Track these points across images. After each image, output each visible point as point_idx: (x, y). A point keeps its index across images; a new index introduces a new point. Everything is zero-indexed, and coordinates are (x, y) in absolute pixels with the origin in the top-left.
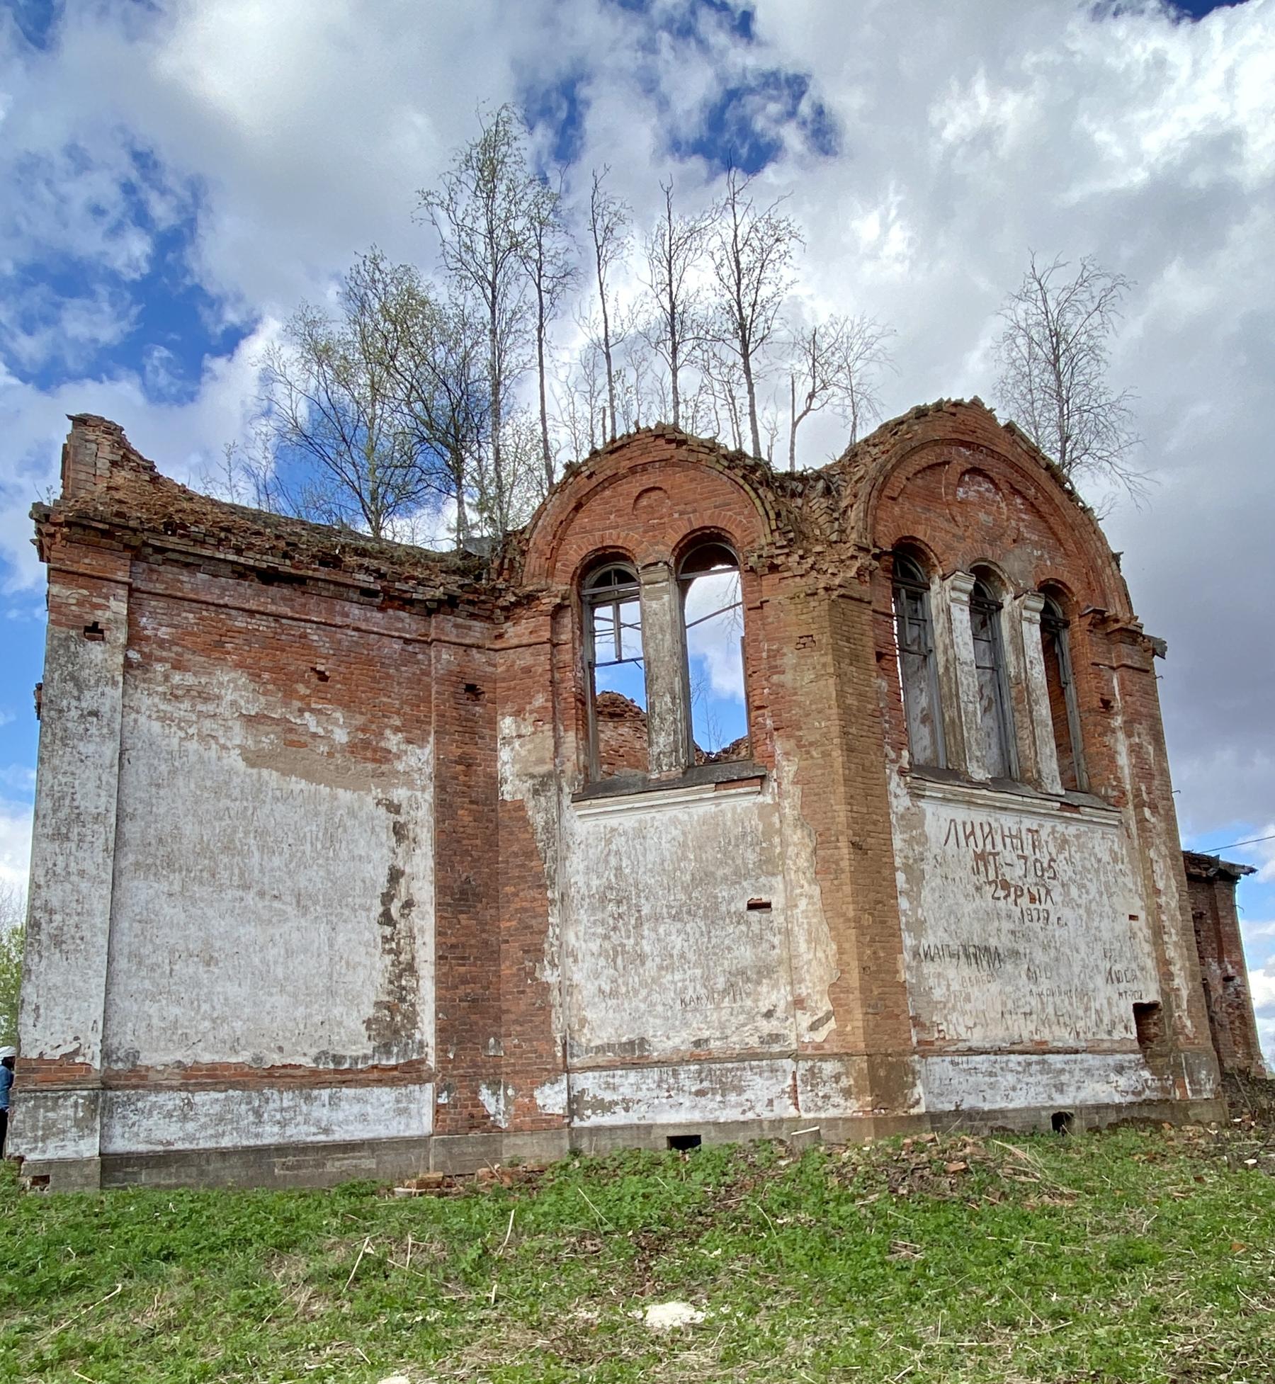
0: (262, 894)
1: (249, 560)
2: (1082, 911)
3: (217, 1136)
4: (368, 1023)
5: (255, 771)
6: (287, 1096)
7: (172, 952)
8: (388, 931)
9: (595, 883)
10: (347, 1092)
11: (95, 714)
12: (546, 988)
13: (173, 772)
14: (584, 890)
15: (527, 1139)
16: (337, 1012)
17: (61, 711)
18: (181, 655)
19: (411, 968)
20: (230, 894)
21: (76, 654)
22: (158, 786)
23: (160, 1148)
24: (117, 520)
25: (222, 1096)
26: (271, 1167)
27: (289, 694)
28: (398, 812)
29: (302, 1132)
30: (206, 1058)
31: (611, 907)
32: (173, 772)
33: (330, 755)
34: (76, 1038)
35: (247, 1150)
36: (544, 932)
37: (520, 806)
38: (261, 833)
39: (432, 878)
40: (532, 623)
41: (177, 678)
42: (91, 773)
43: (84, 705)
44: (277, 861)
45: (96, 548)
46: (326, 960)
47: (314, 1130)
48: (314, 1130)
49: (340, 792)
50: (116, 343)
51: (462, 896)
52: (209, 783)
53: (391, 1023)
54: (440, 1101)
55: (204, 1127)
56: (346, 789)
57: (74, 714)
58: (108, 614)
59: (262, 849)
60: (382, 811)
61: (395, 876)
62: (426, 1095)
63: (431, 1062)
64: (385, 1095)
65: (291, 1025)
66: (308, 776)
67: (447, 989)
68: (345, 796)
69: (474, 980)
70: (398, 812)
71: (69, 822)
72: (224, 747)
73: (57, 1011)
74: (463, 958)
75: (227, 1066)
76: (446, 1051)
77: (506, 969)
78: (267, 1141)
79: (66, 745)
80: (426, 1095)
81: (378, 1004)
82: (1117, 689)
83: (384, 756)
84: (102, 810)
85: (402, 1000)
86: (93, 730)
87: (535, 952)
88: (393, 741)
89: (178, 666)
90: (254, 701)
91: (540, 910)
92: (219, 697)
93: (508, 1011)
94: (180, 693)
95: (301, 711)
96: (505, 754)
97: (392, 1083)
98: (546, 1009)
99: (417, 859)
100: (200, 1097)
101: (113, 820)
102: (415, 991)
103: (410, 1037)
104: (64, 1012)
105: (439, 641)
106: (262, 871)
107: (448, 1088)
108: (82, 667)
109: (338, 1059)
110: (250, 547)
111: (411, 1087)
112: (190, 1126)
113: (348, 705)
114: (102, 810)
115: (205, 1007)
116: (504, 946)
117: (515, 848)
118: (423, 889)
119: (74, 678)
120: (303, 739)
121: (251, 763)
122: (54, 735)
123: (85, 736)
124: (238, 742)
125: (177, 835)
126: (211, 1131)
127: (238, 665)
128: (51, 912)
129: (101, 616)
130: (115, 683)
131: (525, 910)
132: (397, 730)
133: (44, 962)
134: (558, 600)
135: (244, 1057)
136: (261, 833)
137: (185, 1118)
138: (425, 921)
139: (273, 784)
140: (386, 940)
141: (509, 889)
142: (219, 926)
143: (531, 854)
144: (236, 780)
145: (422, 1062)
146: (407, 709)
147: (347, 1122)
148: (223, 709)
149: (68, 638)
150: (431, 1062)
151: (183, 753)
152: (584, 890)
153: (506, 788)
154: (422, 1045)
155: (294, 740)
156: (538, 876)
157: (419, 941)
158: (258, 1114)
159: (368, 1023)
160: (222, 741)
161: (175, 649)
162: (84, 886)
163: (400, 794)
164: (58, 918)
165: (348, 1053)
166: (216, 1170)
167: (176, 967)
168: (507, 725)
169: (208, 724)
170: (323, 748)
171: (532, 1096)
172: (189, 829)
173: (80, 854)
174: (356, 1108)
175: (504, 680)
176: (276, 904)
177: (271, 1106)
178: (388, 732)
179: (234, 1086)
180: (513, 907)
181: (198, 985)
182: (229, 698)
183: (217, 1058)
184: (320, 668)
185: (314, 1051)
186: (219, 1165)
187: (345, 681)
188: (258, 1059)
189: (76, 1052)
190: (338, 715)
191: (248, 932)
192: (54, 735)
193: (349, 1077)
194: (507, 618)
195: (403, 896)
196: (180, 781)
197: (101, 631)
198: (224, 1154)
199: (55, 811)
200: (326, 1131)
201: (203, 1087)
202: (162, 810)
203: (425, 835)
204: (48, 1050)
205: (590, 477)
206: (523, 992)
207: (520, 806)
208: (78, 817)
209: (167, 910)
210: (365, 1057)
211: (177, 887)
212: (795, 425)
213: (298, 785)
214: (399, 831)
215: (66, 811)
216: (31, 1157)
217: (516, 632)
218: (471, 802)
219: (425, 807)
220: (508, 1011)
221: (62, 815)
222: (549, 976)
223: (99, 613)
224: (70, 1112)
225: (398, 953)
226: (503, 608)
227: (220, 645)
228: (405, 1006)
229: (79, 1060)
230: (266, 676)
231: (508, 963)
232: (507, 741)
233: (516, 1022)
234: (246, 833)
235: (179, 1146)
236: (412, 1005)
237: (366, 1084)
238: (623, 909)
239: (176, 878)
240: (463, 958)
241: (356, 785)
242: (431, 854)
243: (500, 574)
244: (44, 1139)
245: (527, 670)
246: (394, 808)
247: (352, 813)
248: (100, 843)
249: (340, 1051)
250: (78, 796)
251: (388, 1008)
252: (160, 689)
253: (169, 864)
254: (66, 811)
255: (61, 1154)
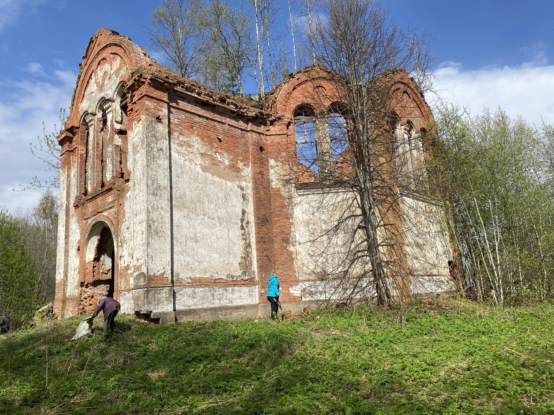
0: (209, 217)
3: (203, 303)
4: (239, 264)
5: (204, 173)
6: (220, 289)
7: (186, 237)
8: (243, 232)
9: (305, 217)
10: (236, 288)
11: (161, 150)
12: (291, 253)
14: (301, 220)
15: (288, 305)
16: (231, 259)
17: (152, 148)
18: (181, 130)
21: (155, 127)
22: (178, 177)
23: (187, 308)
24: (166, 79)
25: (203, 289)
26: (218, 314)
27: (212, 146)
28: (243, 190)
29: (225, 303)
30: (198, 276)
31: (311, 226)
32: (182, 172)
33: (224, 169)
34: (164, 268)
35: (211, 309)
36: (289, 234)
37: (279, 190)
38: (208, 196)
39: (253, 214)
40: (280, 127)
43: (158, 146)
44: (212, 206)
46: (227, 241)
47: (228, 302)
48: (228, 302)
49: (228, 182)
50: (450, 71)
51: (263, 221)
52: (192, 177)
53: (245, 265)
54: (262, 292)
55: (199, 300)
56: (229, 181)
57: (155, 149)
58: (163, 113)
60: (239, 189)
61: (244, 212)
62: (256, 289)
63: (257, 278)
64: (245, 289)
65: (219, 264)
66: (220, 176)
67: (261, 252)
68: (229, 184)
69: (268, 250)
70: (243, 190)
72: (196, 164)
73: (158, 258)
74: (265, 242)
75: (203, 279)
76: (262, 274)
77: (277, 246)
78: (216, 306)
79: (154, 161)
80: (256, 289)
83: (238, 170)
84: (166, 185)
85: (248, 256)
86: (161, 156)
87: (286, 241)
88: (240, 165)
89: (181, 134)
90: (203, 148)
91: (288, 226)
92: (193, 146)
93: (277, 261)
94: (182, 143)
95: (216, 152)
96: (272, 171)
98: (292, 260)
99: (249, 207)
100: (197, 290)
101: (169, 189)
102: (251, 253)
103: (251, 269)
104: (160, 258)
105: (252, 131)
106: (208, 209)
107: (264, 287)
108: (157, 132)
109: (233, 277)
111: (253, 287)
112: (195, 300)
113: (228, 151)
114: (166, 185)
115: (196, 257)
116: (275, 238)
117: (278, 204)
118: (251, 217)
119: (155, 136)
120: (217, 162)
121: (204, 171)
122: (151, 156)
123: (159, 158)
124: (199, 162)
125: (185, 196)
126: (201, 302)
127: (198, 135)
128: (154, 222)
129: (161, 114)
130: (166, 139)
131: (282, 226)
132: (241, 161)
133: (153, 240)
134: (289, 120)
135: (207, 276)
136: (208, 196)
137: (193, 297)
138: (252, 228)
139: (210, 179)
140: (243, 235)
141: (276, 219)
142: (199, 228)
143: (283, 206)
144: (200, 177)
145: (254, 278)
146: (243, 154)
147: (236, 299)
148: (195, 150)
149: (152, 121)
150: (257, 278)
151: (185, 166)
152: (301, 220)
153: (273, 183)
154: (254, 272)
155: (215, 163)
156: (286, 214)
157: (251, 236)
158: (213, 296)
159: (239, 264)
160: (195, 162)
161: (180, 127)
162: (163, 212)
163: (243, 184)
164: (156, 224)
165: (235, 275)
166: (204, 316)
167: (187, 243)
168: (272, 162)
170: (222, 166)
171: (288, 290)
172: (188, 193)
173: (161, 201)
174: (239, 294)
175: (270, 146)
176: (213, 221)
177: (217, 293)
178: (239, 162)
179: (206, 286)
180: (278, 225)
181: (194, 249)
182: (196, 146)
183: (200, 276)
184: (220, 138)
185: (226, 274)
186: (204, 314)
187: (227, 143)
188: (212, 276)
189: (164, 273)
190: (225, 155)
192: (151, 156)
193: (236, 283)
194: (271, 125)
196: (184, 176)
197: (161, 119)
198: (205, 310)
199: (153, 185)
200: (231, 302)
201: (197, 286)
202: (180, 186)
203: (251, 198)
204: (156, 272)
205: (298, 79)
206: (283, 254)
207: (279, 190)
208: (159, 187)
209: (184, 222)
210: (240, 276)
211: (186, 214)
213: (217, 179)
214: (244, 197)
215: (156, 185)
216: (154, 311)
217: (274, 129)
218: (264, 188)
219: (250, 188)
220: (277, 261)
221: (154, 186)
222: (291, 248)
223: (160, 112)
224: (164, 295)
226: (270, 121)
227: (192, 127)
228: (249, 258)
229: (165, 276)
230: (205, 139)
231: (277, 244)
232: (272, 167)
233: (281, 264)
234: (204, 195)
235: (193, 307)
236: (251, 258)
237: (240, 285)
238: (316, 227)
239: (186, 210)
240: (265, 242)
241: (232, 181)
242: (252, 205)
243: (268, 109)
244: (158, 304)
245: (279, 143)
246: (242, 189)
247: (231, 190)
248: (166, 197)
249: (233, 274)
250: (159, 180)
251: (244, 259)
252: (177, 142)
254: (156, 185)
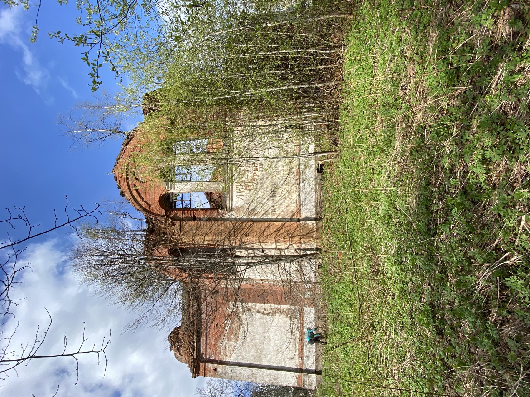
1: (195, 339)
2: (359, 135)
8: (271, 314)
11: (231, 371)
13: (241, 356)
19: (278, 309)
20: (264, 346)
32: (241, 356)
41: (222, 354)
42: (243, 372)
44: (257, 337)
45: (199, 369)
59: (255, 340)
61: (259, 312)
71: (253, 376)
81: (287, 317)
82: (308, 86)
85: (285, 312)
89: (220, 353)
97: (303, 315)
100: (305, 354)
110: (193, 340)
119: (225, 374)
123: (236, 373)
129: (212, 368)
162: (265, 374)
169: (231, 349)
172: (252, 353)
191: (272, 343)
195: (262, 310)
208: (252, 375)
209: (269, 358)
212: (72, 355)
225: (276, 312)
239: (262, 356)
253: (260, 357)
255: (315, 381)
